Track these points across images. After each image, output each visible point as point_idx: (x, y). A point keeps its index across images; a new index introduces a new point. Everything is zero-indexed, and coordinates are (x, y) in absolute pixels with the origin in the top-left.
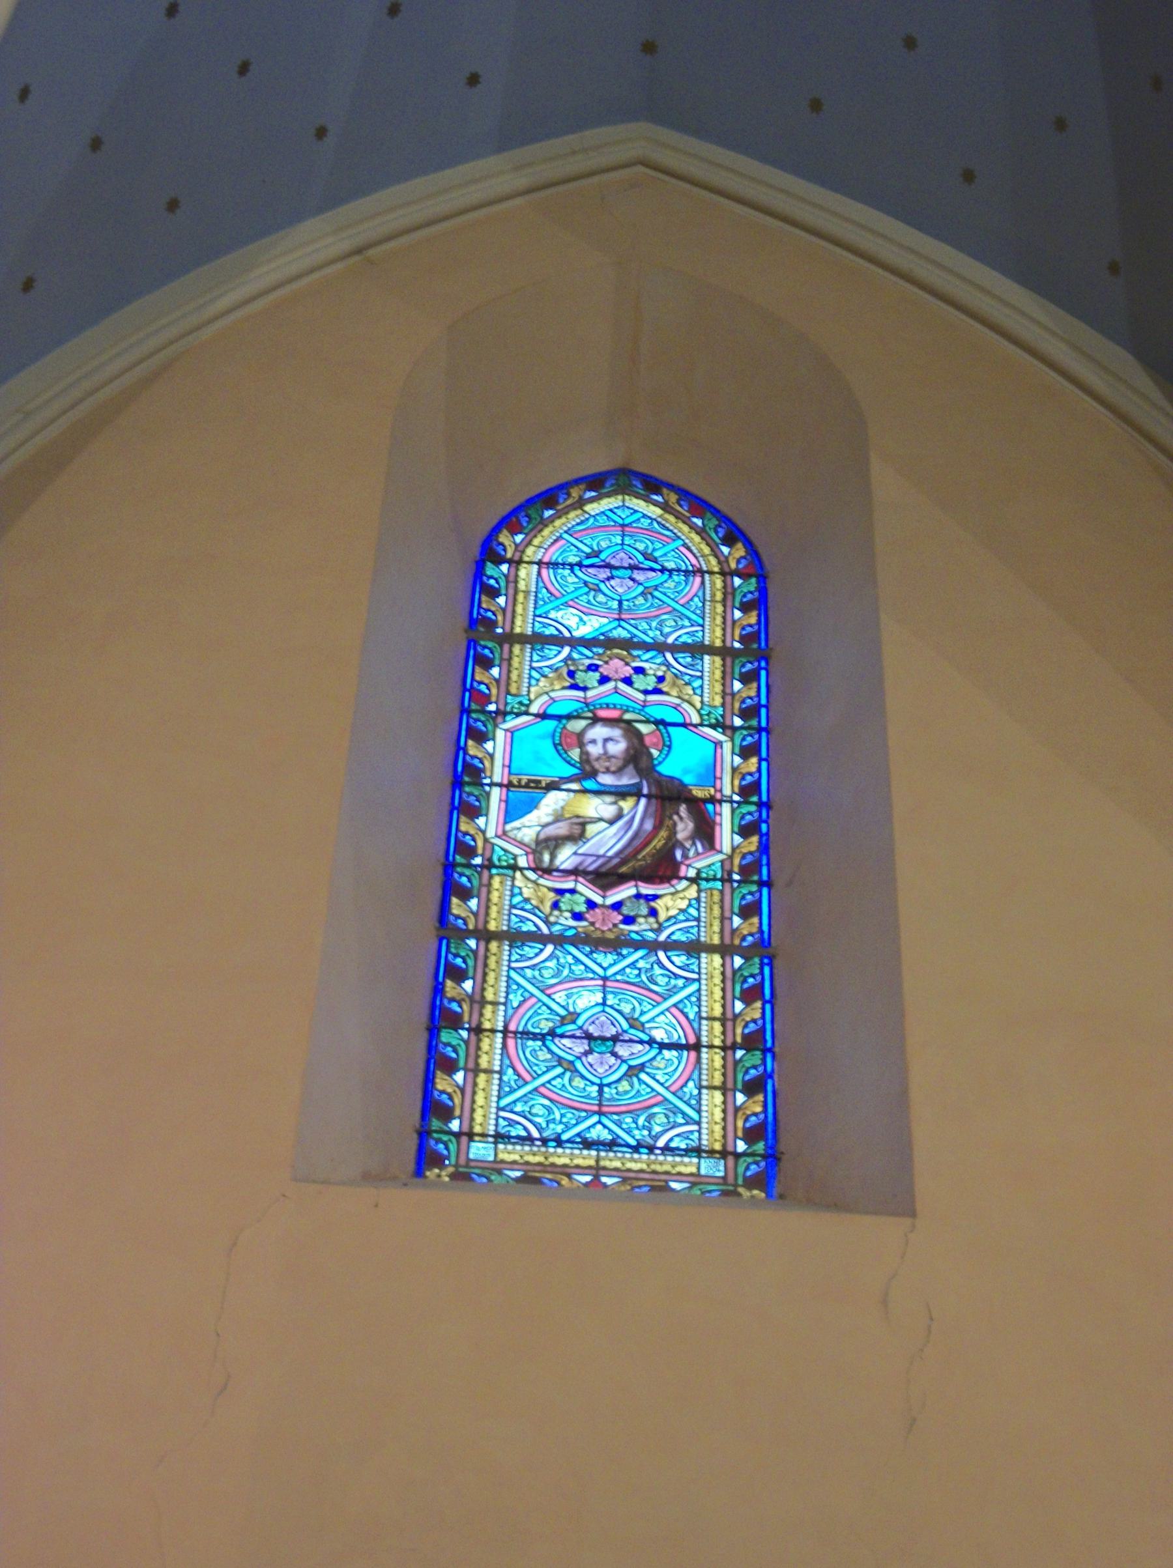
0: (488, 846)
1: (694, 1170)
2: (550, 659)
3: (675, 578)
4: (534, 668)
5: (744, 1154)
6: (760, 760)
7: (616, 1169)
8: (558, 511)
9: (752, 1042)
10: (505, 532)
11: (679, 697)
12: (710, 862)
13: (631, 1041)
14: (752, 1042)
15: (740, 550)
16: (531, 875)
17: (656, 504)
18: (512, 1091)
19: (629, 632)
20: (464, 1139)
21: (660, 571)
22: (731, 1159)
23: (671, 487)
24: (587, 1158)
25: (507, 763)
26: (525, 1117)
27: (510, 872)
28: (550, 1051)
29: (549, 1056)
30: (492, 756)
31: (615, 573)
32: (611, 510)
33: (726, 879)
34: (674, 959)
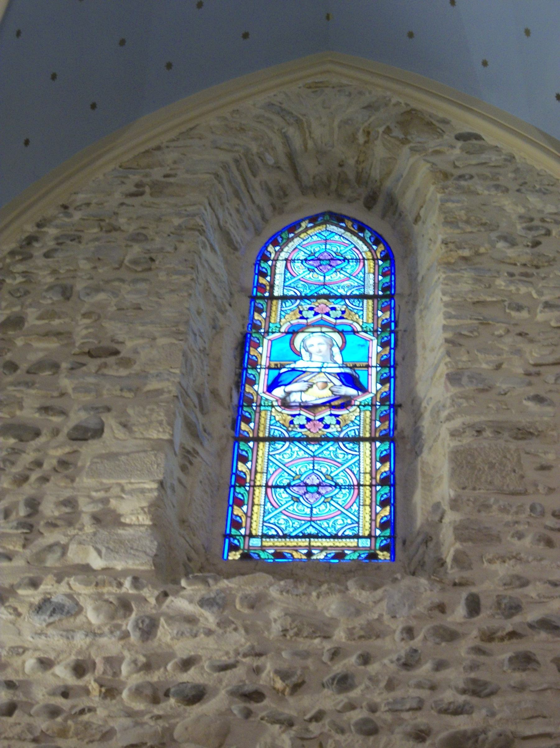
0: (259, 397)
1: (356, 545)
2: (278, 449)
3: (351, 263)
4: (283, 311)
5: (379, 536)
6: (391, 349)
7: (318, 547)
8: (295, 234)
9: (384, 482)
10: (271, 246)
11: (352, 320)
12: (367, 398)
13: (326, 486)
14: (384, 482)
15: (381, 248)
16: (279, 409)
17: (341, 227)
18: (269, 513)
19: (328, 291)
20: (247, 538)
21: (334, 486)
22: (373, 539)
23: (349, 218)
24: (304, 542)
25: (269, 355)
26: (275, 525)
27: (270, 408)
28: (287, 493)
29: (287, 496)
30: (261, 354)
31: (322, 262)
32: (319, 233)
33: (373, 405)
34: (347, 445)
